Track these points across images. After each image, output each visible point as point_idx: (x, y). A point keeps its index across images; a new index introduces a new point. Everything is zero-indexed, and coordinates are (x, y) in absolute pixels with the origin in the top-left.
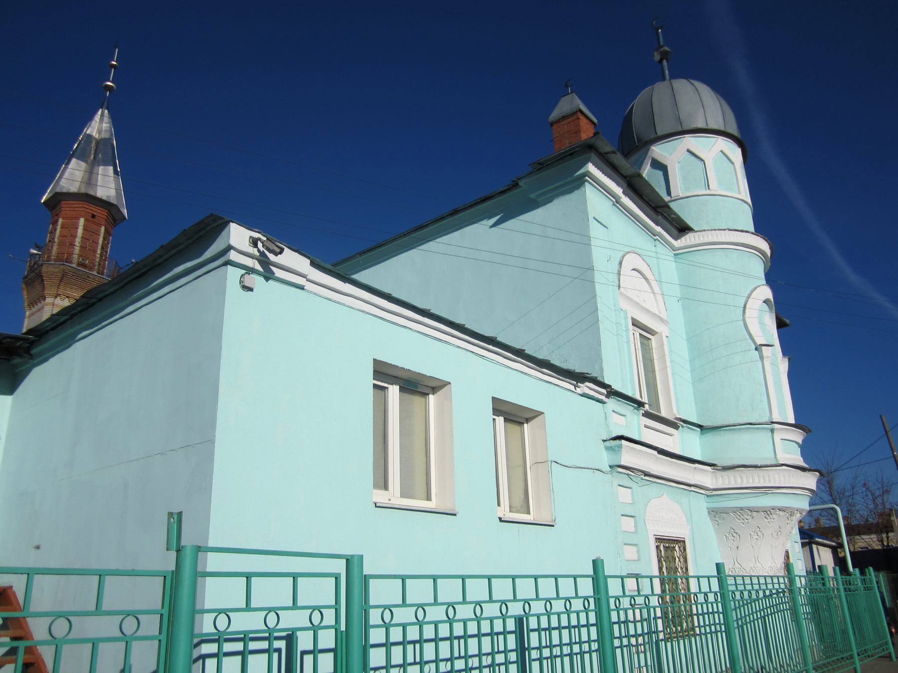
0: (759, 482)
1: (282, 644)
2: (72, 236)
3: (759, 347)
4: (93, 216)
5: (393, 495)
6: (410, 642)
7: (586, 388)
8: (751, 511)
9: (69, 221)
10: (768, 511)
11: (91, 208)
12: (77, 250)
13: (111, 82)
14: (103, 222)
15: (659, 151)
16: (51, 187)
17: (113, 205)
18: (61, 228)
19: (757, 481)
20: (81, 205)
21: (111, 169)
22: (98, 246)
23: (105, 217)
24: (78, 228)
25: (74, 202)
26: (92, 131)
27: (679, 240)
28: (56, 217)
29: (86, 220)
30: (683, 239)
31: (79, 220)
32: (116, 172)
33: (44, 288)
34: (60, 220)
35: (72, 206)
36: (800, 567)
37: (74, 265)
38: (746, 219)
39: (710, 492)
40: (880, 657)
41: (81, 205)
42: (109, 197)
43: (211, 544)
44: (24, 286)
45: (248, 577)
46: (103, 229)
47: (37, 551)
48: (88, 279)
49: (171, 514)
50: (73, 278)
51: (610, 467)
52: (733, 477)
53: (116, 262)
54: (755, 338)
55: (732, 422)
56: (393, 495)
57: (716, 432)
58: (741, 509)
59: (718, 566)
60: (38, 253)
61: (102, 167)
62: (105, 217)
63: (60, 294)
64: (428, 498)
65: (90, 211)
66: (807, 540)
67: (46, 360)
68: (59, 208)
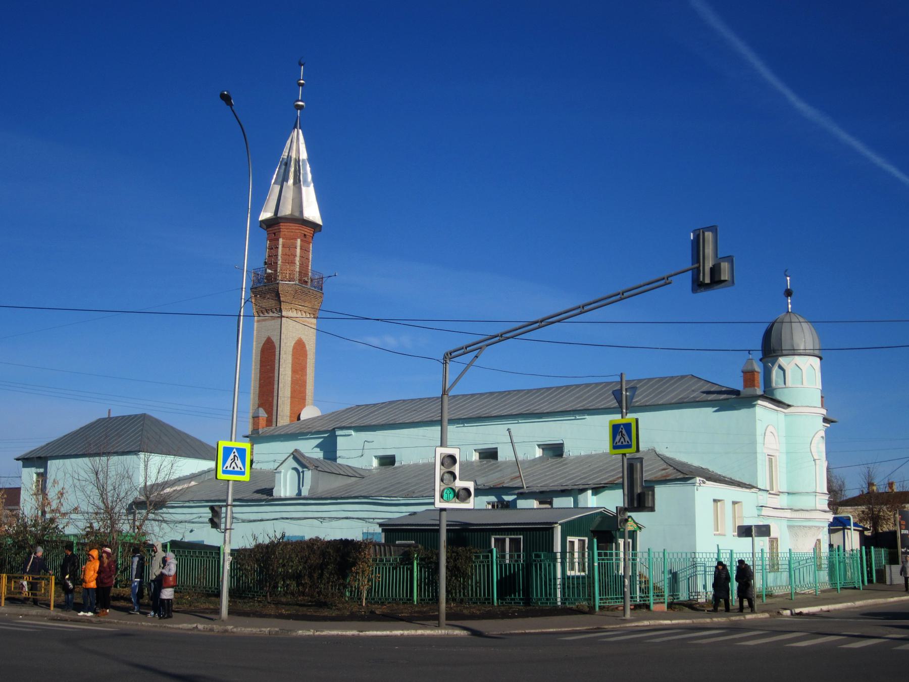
4: (305, 235)
7: (754, 490)
10: (810, 527)
15: (782, 361)
18: (282, 247)
20: (297, 228)
29: (301, 240)
34: (281, 240)
35: (290, 228)
36: (825, 548)
38: (818, 402)
39: (789, 519)
40: (687, 475)
41: (297, 228)
51: (758, 515)
55: (800, 491)
57: (794, 495)
58: (800, 526)
59: (790, 549)
64: (718, 531)
66: (842, 527)
67: (615, 490)
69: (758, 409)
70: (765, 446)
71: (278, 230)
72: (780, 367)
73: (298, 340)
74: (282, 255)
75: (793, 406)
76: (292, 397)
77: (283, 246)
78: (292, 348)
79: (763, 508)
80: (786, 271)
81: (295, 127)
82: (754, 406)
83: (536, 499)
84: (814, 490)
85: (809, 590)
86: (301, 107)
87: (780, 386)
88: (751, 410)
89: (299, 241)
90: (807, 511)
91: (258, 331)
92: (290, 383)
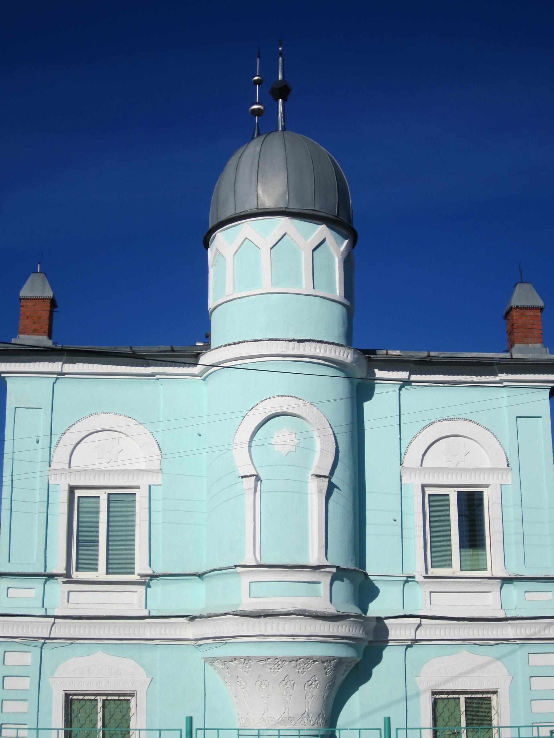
13: (258, 104)
70: (53, 467)
86: (257, 112)
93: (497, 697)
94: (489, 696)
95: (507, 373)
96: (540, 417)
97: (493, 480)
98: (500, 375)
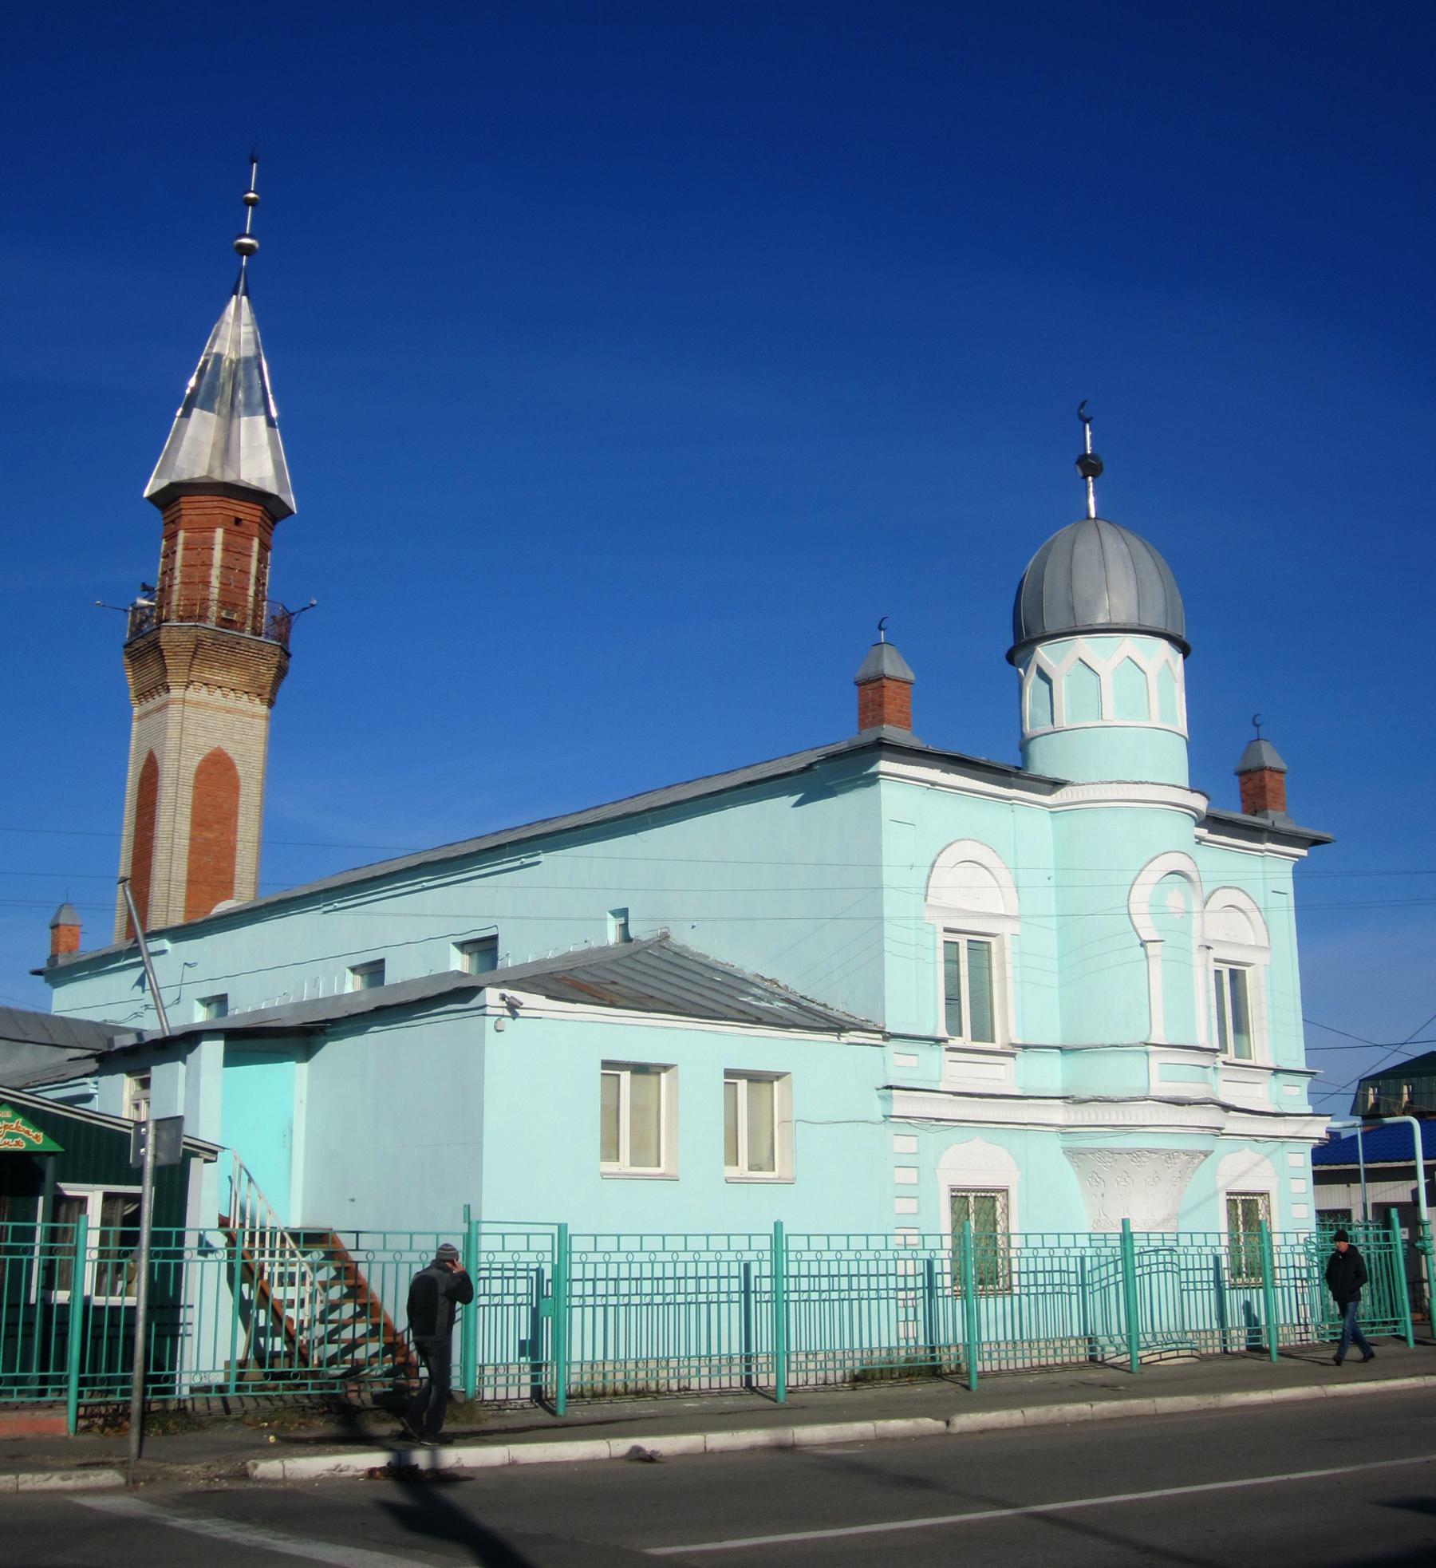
0: (1103, 1119)
1: (533, 1274)
2: (203, 564)
3: (1144, 943)
4: (238, 521)
5: (624, 1164)
6: (633, 1279)
8: (1112, 1153)
9: (197, 535)
10: (1136, 1153)
11: (232, 506)
12: (215, 582)
13: (250, 236)
14: (255, 529)
15: (1044, 654)
16: (159, 462)
17: (270, 496)
19: (1115, 1118)
21: (261, 420)
22: (249, 580)
23: (258, 520)
24: (213, 549)
25: (202, 498)
26: (223, 346)
27: (1054, 795)
28: (173, 526)
29: (227, 532)
30: (1059, 793)
31: (215, 532)
32: (270, 423)
33: (164, 671)
35: (201, 505)
37: (211, 625)
39: (1064, 1129)
42: (261, 479)
43: (483, 1220)
44: (126, 661)
45: (503, 1235)
46: (256, 542)
47: (353, 1203)
48: (237, 646)
49: (465, 1206)
50: (213, 647)
51: (884, 1116)
52: (1087, 1114)
53: (284, 607)
54: (1139, 931)
55: (1098, 1042)
56: (624, 1164)
57: (1078, 1054)
58: (1099, 1150)
60: (150, 603)
61: (245, 418)
62: (258, 520)
63: (193, 681)
64: (659, 1165)
65: (232, 513)
67: (341, 1039)
68: (176, 508)
69: (885, 788)
70: (930, 900)
71: (177, 514)
72: (1042, 675)
73: (212, 754)
74: (182, 566)
75: (1071, 784)
76: (191, 882)
77: (186, 548)
78: (193, 771)
79: (895, 1092)
80: (1082, 405)
81: (236, 292)
82: (873, 780)
83: (130, 1073)
84: (1143, 1039)
85: (1145, 1353)
86: (247, 250)
87: (1040, 730)
88: (871, 789)
89: (219, 534)
90: (1112, 1101)
91: (139, 740)
92: (186, 851)
93: (256, 1187)
94: (1255, 1198)
95: (1274, 842)
96: (1274, 892)
97: (1005, 928)
98: (1267, 844)
